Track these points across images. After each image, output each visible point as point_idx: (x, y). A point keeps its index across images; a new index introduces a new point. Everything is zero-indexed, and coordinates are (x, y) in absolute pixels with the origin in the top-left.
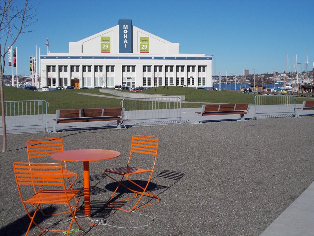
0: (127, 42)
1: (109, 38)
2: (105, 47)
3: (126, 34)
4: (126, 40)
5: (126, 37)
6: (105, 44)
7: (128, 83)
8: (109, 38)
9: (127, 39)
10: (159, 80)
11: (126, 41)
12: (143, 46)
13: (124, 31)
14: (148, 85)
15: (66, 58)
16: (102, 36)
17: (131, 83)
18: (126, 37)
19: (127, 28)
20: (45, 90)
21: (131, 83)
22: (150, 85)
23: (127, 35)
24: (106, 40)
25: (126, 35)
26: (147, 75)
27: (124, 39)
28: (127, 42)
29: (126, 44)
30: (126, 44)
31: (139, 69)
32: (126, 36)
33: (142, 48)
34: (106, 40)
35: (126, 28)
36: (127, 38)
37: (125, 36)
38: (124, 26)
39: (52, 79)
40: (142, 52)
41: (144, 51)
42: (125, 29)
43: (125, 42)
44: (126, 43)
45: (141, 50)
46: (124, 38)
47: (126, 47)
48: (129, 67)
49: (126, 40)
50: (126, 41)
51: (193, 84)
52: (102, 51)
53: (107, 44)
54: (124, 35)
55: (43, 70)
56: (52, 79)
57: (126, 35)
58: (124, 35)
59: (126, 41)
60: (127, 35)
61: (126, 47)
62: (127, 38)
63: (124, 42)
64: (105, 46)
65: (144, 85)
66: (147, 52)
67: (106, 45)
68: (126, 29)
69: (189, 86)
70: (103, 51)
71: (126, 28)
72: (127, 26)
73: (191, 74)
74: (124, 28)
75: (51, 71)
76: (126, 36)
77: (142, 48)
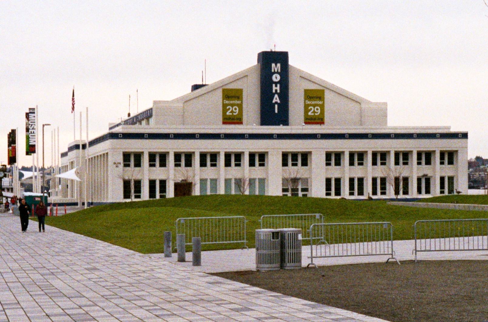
0: (279, 102)
1: (241, 91)
2: (314, 112)
3: (276, 83)
4: (276, 96)
5: (276, 90)
6: (232, 105)
7: (293, 190)
8: (241, 91)
10: (336, 184)
11: (278, 98)
12: (311, 109)
13: (274, 76)
14: (136, 197)
15: (241, 136)
16: (224, 87)
18: (276, 90)
19: (279, 71)
20: (72, 211)
22: (139, 197)
23: (278, 85)
24: (317, 98)
25: (276, 86)
27: (274, 94)
28: (279, 102)
29: (276, 106)
30: (276, 106)
32: (276, 88)
33: (228, 113)
34: (317, 98)
35: (276, 71)
36: (278, 91)
37: (274, 88)
38: (273, 65)
39: (132, 184)
40: (309, 121)
41: (313, 121)
42: (275, 73)
44: (276, 103)
45: (307, 117)
46: (274, 91)
47: (276, 111)
48: (295, 156)
49: (276, 96)
52: (307, 121)
53: (317, 105)
54: (274, 85)
56: (132, 184)
57: (276, 86)
58: (274, 85)
60: (278, 85)
61: (276, 111)
62: (278, 91)
63: (274, 102)
64: (230, 110)
65: (327, 194)
66: (320, 121)
67: (316, 108)
68: (277, 73)
69: (352, 197)
70: (227, 120)
71: (276, 71)
72: (279, 65)
74: (273, 71)
76: (276, 88)
77: (228, 113)
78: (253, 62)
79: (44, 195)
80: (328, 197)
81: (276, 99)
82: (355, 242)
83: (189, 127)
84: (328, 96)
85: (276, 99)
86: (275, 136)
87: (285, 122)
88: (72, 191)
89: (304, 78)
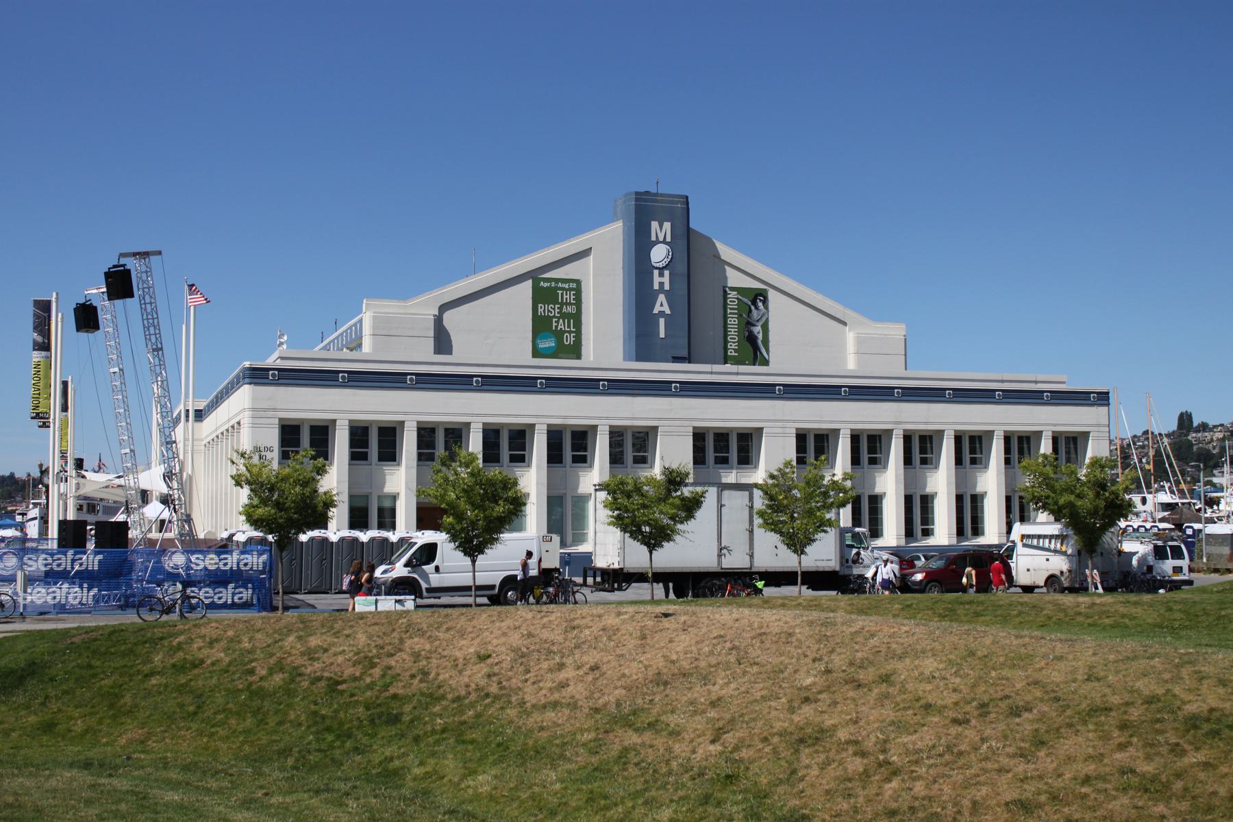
0: (668, 311)
9: (667, 294)
18: (661, 284)
29: (662, 321)
30: (662, 321)
44: (662, 313)
46: (656, 287)
47: (662, 335)
61: (662, 335)
62: (667, 287)
72: (667, 225)
81: (662, 305)
85: (662, 305)
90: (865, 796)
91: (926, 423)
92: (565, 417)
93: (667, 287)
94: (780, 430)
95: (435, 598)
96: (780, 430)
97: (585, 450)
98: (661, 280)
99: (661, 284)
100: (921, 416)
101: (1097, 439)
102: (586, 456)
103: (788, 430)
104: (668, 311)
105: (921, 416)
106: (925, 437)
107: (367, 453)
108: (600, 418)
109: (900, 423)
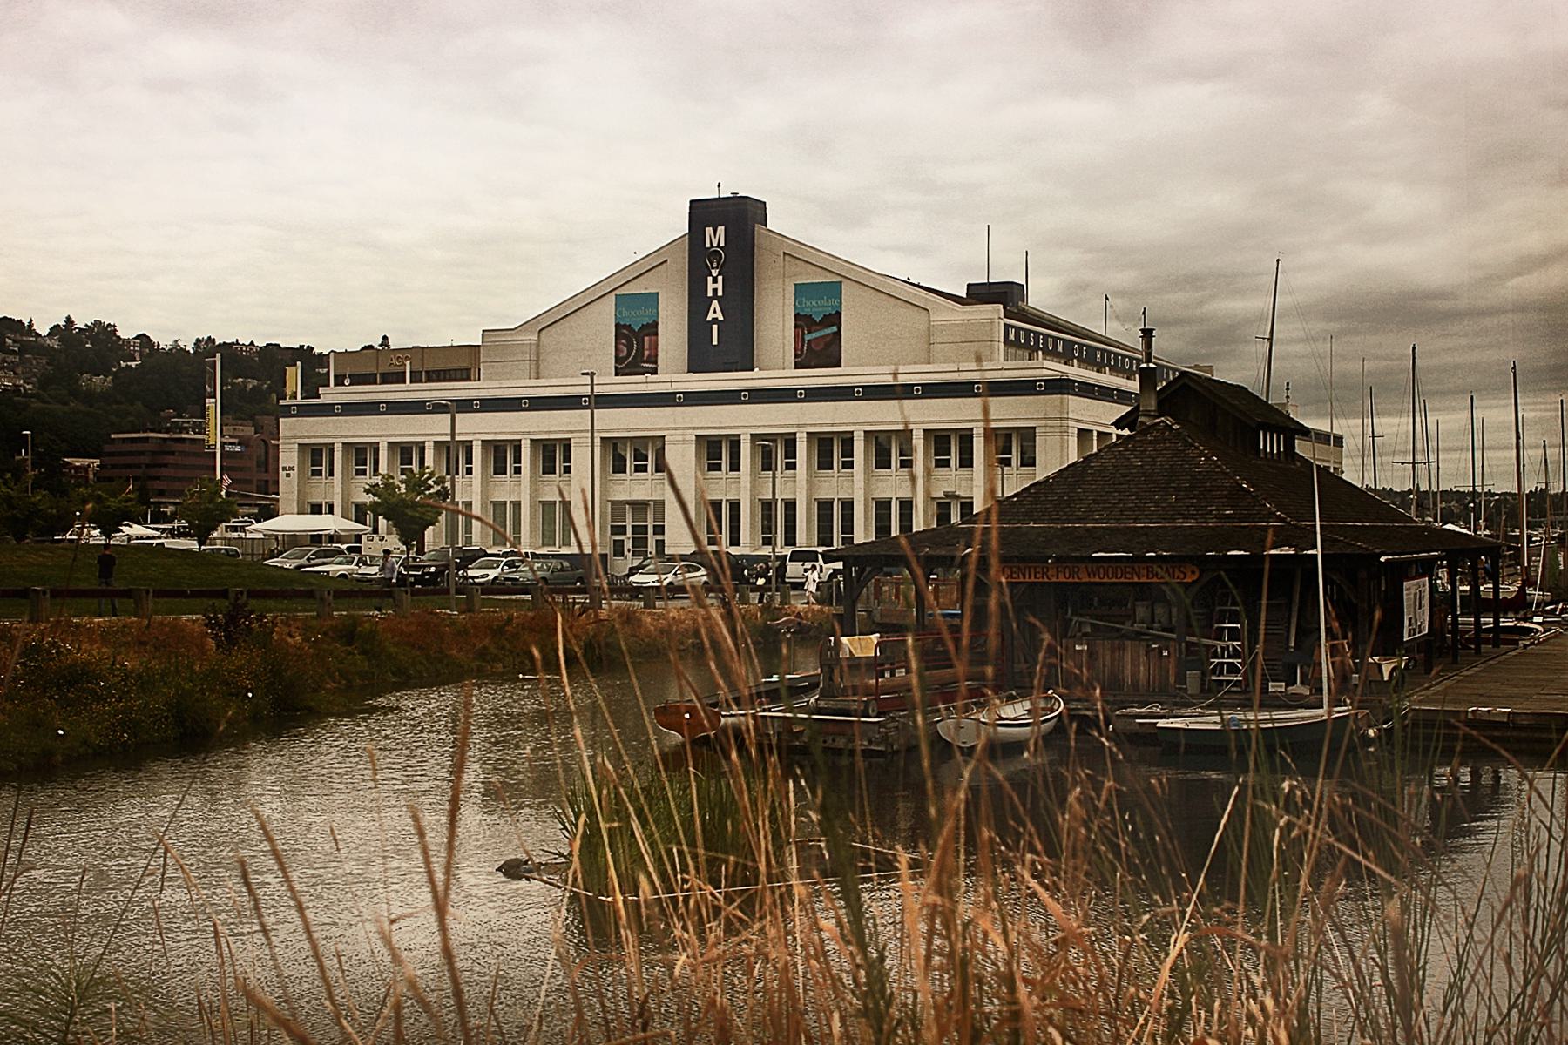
0: (721, 318)
4: (715, 304)
9: (719, 299)
11: (718, 310)
17: (650, 530)
18: (715, 291)
21: (650, 530)
26: (723, 487)
27: (712, 299)
29: (715, 327)
30: (715, 327)
31: (682, 458)
38: (709, 230)
43: (715, 316)
44: (715, 320)
46: (710, 294)
47: (715, 342)
49: (715, 304)
50: (715, 312)
51: (735, 541)
55: (284, 469)
59: (715, 312)
61: (715, 342)
62: (720, 293)
72: (721, 230)
73: (833, 486)
75: (952, 463)
78: (680, 225)
79: (1256, 716)
80: (296, 468)
81: (715, 312)
82: (1255, 707)
83: (936, 365)
84: (847, 290)
85: (715, 312)
86: (978, 388)
87: (746, 363)
88: (452, 526)
89: (795, 253)
90: (485, 648)
91: (832, 425)
92: (495, 434)
93: (720, 293)
94: (681, 438)
95: (1303, 718)
96: (681, 438)
97: (911, 455)
98: (715, 286)
99: (715, 291)
100: (885, 415)
101: (1045, 434)
102: (911, 460)
103: (687, 438)
104: (721, 318)
105: (885, 415)
106: (772, 438)
107: (911, 460)
108: (523, 433)
109: (805, 425)
